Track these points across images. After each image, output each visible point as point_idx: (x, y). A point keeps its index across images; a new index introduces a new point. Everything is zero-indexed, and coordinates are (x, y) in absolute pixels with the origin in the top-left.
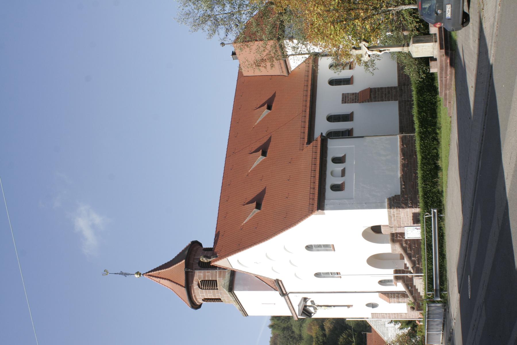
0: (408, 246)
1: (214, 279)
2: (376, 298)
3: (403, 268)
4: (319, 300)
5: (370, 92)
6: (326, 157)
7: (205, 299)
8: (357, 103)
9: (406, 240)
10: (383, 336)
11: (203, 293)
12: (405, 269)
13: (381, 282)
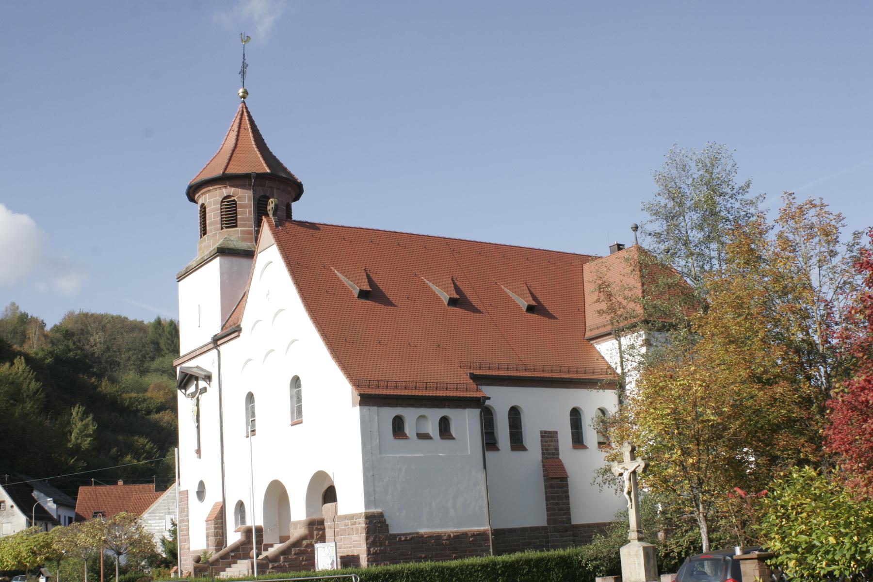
2: (213, 497)
3: (266, 540)
4: (209, 400)
5: (560, 478)
6: (449, 407)
7: (205, 208)
8: (542, 457)
9: (313, 546)
11: (214, 205)
12: (265, 545)
13: (240, 506)
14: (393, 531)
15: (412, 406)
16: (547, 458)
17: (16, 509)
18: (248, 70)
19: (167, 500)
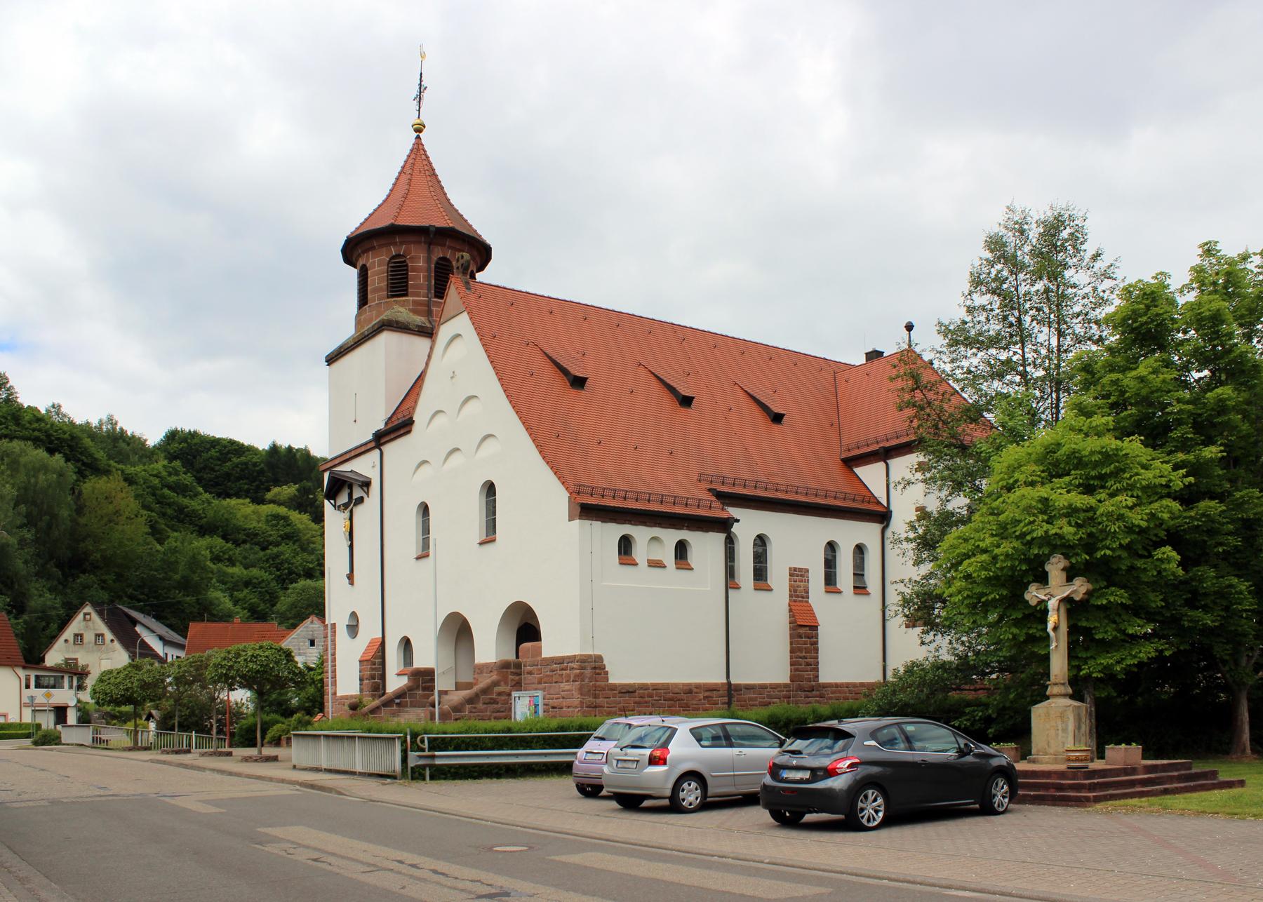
0: (494, 696)
1: (410, 290)
2: (369, 631)
4: (366, 514)
6: (689, 528)
7: (367, 270)
9: (510, 695)
11: (379, 266)
13: (406, 644)
14: (614, 679)
15: (644, 523)
16: (795, 601)
17: (117, 645)
18: (425, 95)
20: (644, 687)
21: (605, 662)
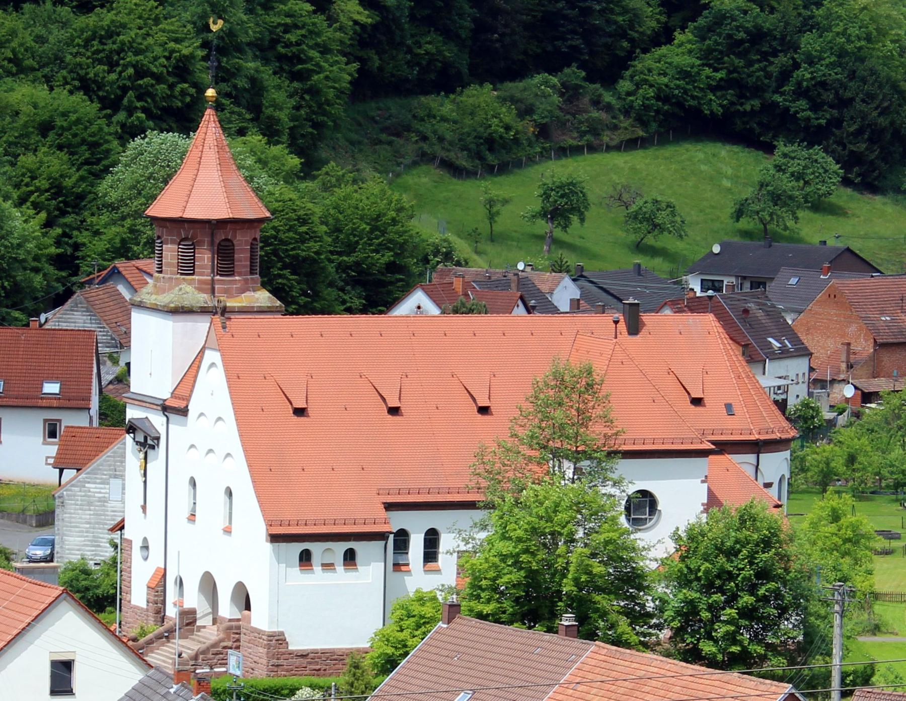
2: (156, 560)
6: (355, 540)
10: (89, 470)
14: (291, 648)
19: (114, 457)
20: (315, 652)
21: (286, 636)
